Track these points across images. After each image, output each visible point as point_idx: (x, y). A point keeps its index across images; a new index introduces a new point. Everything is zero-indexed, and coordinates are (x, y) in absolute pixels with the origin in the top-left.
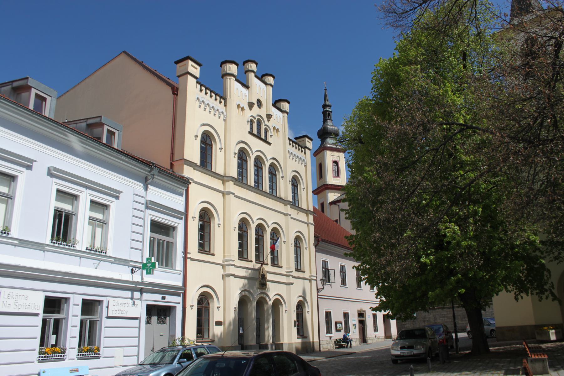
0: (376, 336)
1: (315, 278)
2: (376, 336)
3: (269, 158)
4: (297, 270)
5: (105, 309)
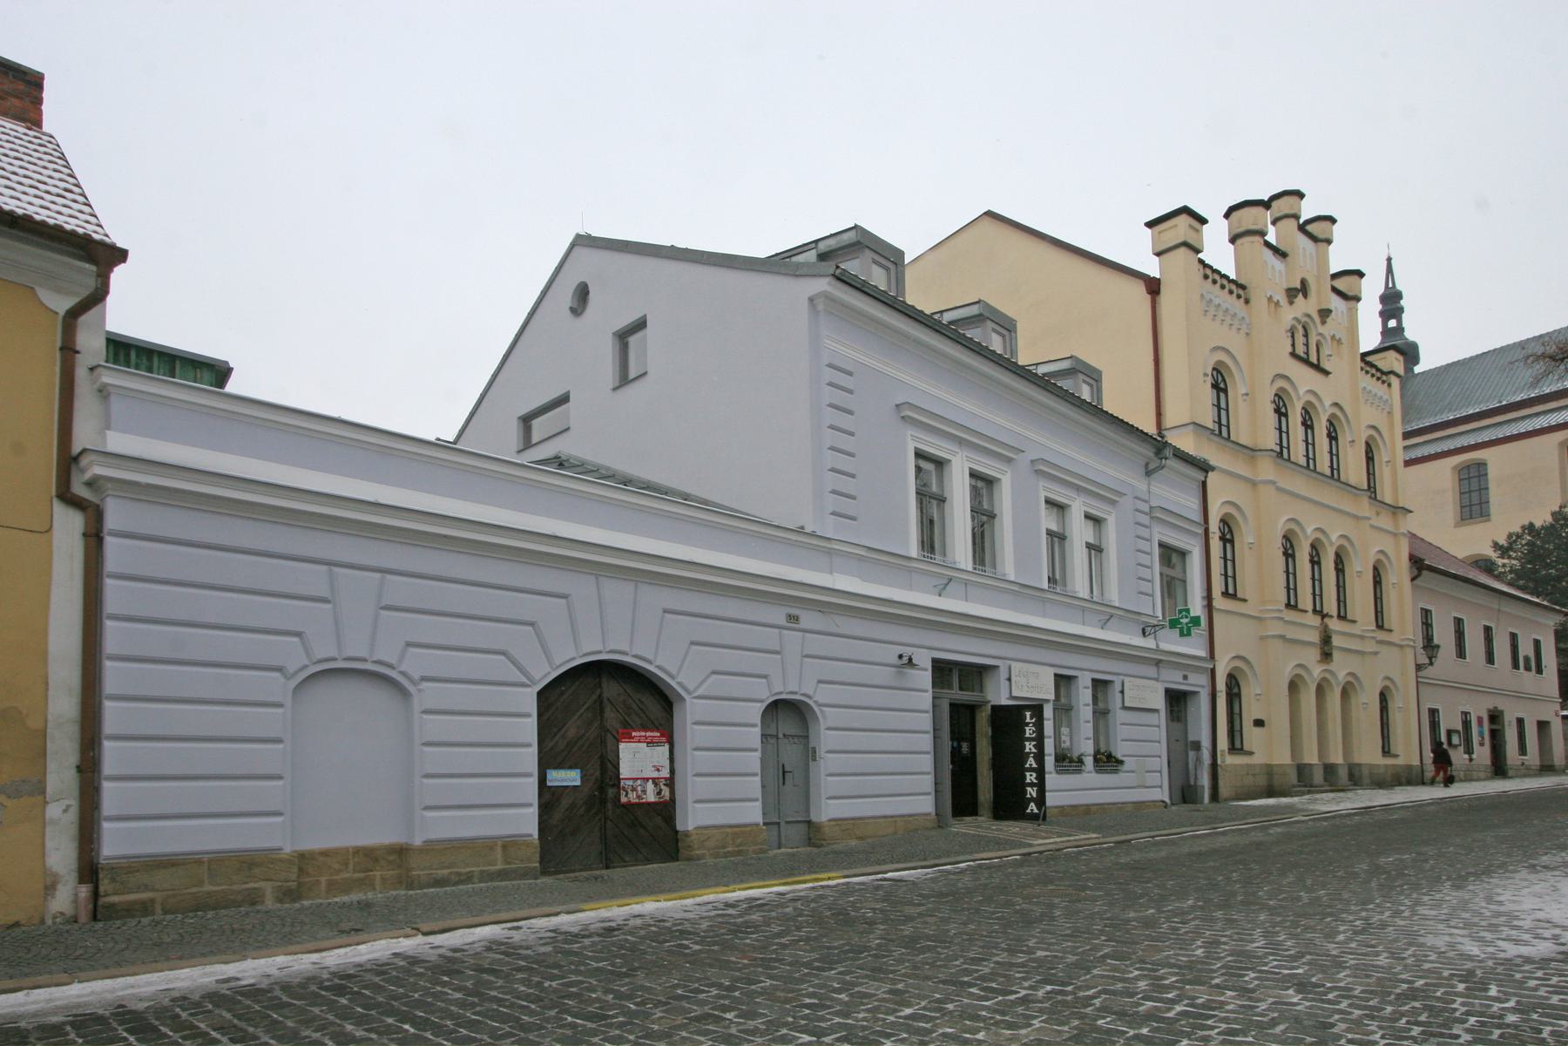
0: (1523, 764)
1: (1412, 644)
2: (1523, 764)
3: (1327, 403)
4: (1380, 626)
5: (1004, 684)
